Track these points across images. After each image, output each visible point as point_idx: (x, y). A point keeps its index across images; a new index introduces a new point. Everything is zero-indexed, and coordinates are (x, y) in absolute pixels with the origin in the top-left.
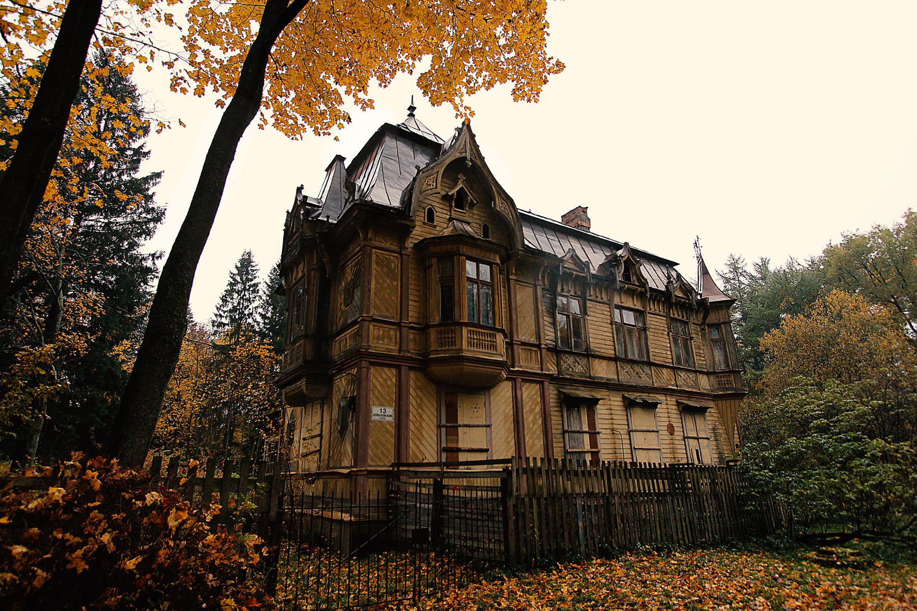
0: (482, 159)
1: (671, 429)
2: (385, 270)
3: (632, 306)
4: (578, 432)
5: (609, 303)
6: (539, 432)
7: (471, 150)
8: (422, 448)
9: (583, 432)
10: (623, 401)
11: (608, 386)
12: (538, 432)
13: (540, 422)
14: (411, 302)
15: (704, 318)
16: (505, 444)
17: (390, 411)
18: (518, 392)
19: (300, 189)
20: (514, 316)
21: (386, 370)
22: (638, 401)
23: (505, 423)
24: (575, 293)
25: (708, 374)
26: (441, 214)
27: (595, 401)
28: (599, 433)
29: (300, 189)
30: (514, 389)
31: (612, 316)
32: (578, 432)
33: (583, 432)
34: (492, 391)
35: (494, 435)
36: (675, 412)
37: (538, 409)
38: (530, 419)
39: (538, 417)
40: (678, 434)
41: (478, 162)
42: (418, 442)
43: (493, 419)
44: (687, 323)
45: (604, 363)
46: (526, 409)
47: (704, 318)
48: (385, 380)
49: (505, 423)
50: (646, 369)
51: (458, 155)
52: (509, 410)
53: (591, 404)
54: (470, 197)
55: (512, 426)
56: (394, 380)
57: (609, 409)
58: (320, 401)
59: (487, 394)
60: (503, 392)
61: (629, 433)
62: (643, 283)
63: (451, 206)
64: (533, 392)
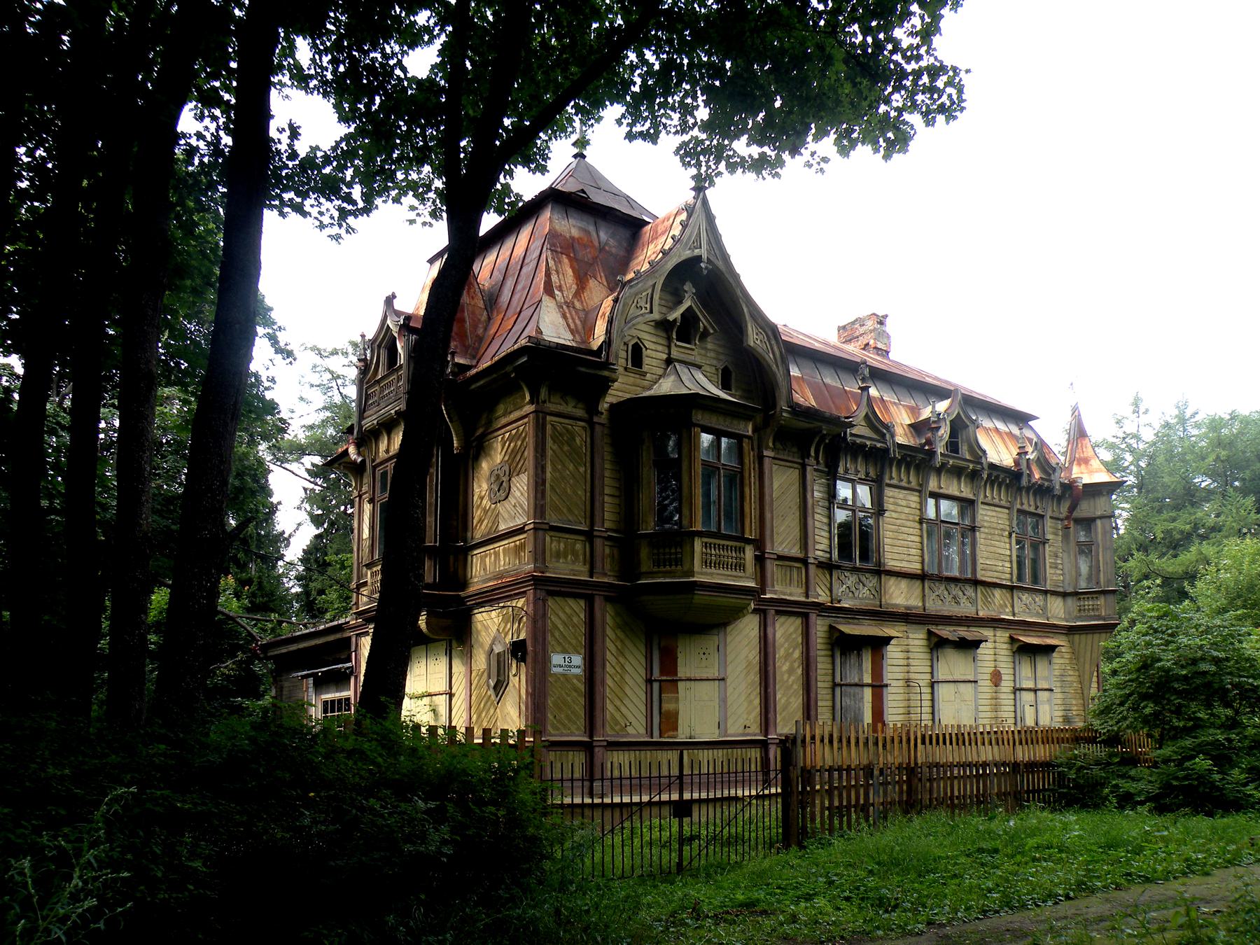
0: (726, 258)
1: (996, 678)
2: (566, 448)
3: (957, 493)
4: (856, 685)
5: (920, 490)
6: (797, 687)
7: (709, 242)
8: (623, 709)
9: (863, 686)
10: (928, 639)
11: (907, 618)
12: (795, 687)
13: (800, 671)
14: (607, 499)
15: (1072, 509)
16: (746, 704)
17: (577, 660)
18: (770, 630)
19: (390, 301)
20: (768, 515)
21: (571, 602)
22: (950, 639)
23: (748, 674)
24: (867, 474)
25: (1064, 595)
26: (654, 354)
27: (887, 640)
28: (886, 686)
29: (390, 301)
30: (764, 626)
31: (922, 507)
32: (856, 685)
33: (863, 686)
34: (729, 629)
35: (730, 690)
36: (1006, 652)
37: (797, 654)
38: (785, 668)
39: (796, 665)
40: (1007, 684)
41: (720, 264)
42: (618, 703)
43: (729, 669)
44: (1042, 516)
45: (904, 583)
46: (780, 653)
47: (1072, 509)
48: (569, 617)
49: (748, 674)
50: (970, 591)
51: (687, 254)
52: (754, 655)
53: (879, 644)
54: (703, 323)
55: (757, 679)
56: (582, 616)
57: (905, 653)
58: (444, 643)
59: (722, 635)
60: (746, 631)
61: (932, 685)
62: (978, 453)
63: (669, 339)
64: (792, 629)
